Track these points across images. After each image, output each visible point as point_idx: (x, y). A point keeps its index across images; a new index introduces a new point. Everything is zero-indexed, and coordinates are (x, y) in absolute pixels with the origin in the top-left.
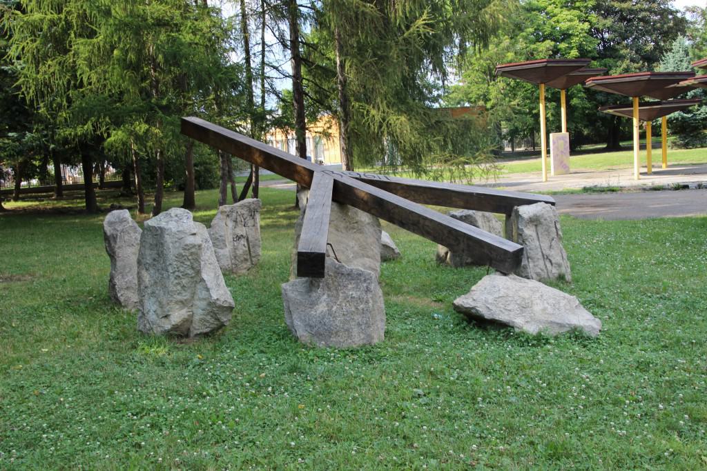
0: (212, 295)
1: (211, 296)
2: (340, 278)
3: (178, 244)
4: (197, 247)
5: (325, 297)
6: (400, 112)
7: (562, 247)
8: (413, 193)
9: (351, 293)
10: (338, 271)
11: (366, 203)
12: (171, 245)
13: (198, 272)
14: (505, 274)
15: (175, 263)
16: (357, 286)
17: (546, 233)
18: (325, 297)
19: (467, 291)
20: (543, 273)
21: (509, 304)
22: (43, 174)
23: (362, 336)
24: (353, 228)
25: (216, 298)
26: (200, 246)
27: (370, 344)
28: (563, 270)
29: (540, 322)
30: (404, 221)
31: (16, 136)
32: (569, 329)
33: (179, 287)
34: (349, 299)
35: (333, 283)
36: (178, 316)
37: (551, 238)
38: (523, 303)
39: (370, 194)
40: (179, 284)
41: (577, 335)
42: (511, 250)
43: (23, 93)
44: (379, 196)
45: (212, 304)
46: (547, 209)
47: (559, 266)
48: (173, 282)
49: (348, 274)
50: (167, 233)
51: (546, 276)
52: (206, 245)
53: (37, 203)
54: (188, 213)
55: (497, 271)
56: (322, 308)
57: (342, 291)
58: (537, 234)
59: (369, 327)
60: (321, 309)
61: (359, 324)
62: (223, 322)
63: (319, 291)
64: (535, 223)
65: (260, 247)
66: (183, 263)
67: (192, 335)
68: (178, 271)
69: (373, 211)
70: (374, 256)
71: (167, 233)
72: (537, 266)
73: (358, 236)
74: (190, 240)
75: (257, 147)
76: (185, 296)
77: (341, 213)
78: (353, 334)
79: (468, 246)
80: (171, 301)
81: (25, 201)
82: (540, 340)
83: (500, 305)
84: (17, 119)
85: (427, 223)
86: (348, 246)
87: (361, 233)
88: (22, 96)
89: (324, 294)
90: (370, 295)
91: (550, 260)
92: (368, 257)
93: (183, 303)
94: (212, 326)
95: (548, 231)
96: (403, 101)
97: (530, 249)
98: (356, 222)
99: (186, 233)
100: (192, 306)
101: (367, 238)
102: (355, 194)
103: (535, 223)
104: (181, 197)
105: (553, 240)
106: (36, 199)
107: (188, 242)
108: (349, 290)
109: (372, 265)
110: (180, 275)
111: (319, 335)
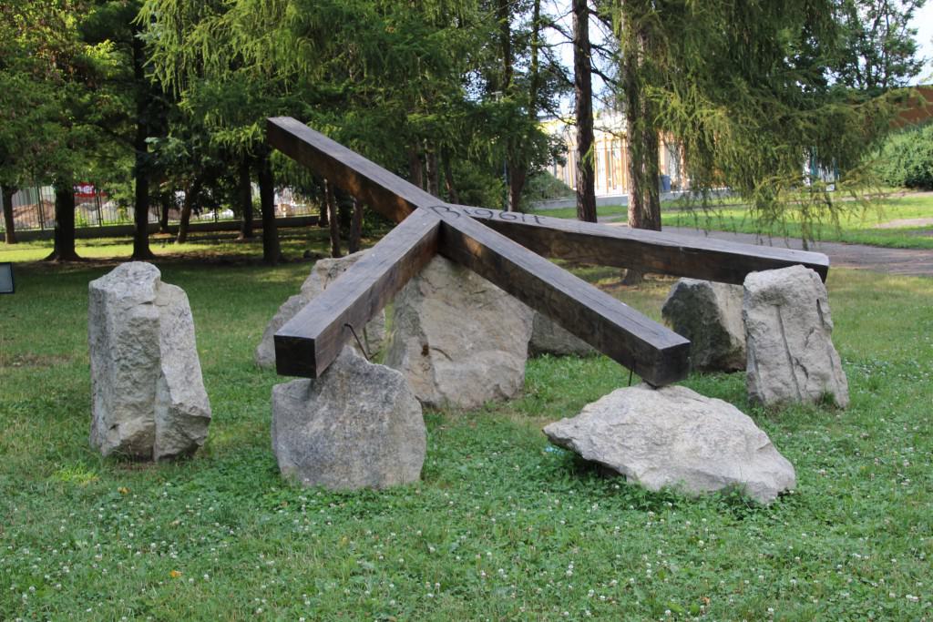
0: (173, 398)
1: (172, 400)
2: (354, 379)
3: (123, 317)
4: (151, 323)
5: (325, 408)
6: (718, 102)
7: (832, 345)
8: (576, 245)
9: (361, 404)
10: (354, 369)
11: (480, 260)
12: (114, 317)
13: (157, 362)
14: (655, 388)
15: (119, 346)
16: (374, 393)
17: (798, 319)
18: (325, 408)
19: (575, 409)
20: (785, 389)
21: (630, 438)
22: (242, 203)
23: (366, 473)
24: (477, 301)
25: (178, 402)
26: (155, 321)
27: (378, 486)
28: (831, 386)
29: (678, 470)
30: (526, 293)
31: (155, 142)
32: (723, 486)
33: (128, 384)
34: (356, 414)
35: (342, 387)
36: (130, 427)
37: (808, 328)
38: (657, 436)
39: (485, 247)
40: (127, 378)
41: (736, 501)
42: (660, 344)
43: (157, 77)
44: (496, 251)
45: (174, 411)
46: (801, 277)
47: (824, 378)
48: (118, 375)
49: (367, 375)
50: (109, 299)
51: (794, 394)
52: (180, 322)
53: (204, 247)
54: (153, 270)
55: (644, 381)
56: (317, 426)
57: (351, 401)
58: (781, 322)
59: (377, 459)
60: (315, 428)
61: (364, 455)
62: (194, 441)
63: (319, 398)
64: (775, 302)
65: (383, 326)
66: (131, 346)
67: (156, 457)
68: (125, 359)
69: (489, 274)
70: (515, 348)
71: (109, 299)
72: (775, 376)
73: (488, 314)
74: (142, 312)
75: (353, 167)
76: (140, 397)
77: (454, 276)
78: (353, 470)
79: (606, 338)
80: (119, 404)
81: (197, 243)
82: (657, 501)
83: (615, 437)
84: (160, 116)
85: (553, 296)
86: (464, 329)
87: (491, 309)
88: (156, 80)
89: (324, 404)
90: (388, 409)
91: (802, 366)
92: (503, 349)
93: (138, 408)
94: (180, 445)
95: (801, 316)
96: (722, 83)
97: (760, 347)
98: (483, 292)
99: (135, 301)
100: (153, 412)
101: (502, 318)
102: (465, 247)
103: (775, 302)
104: (50, 246)
105: (812, 332)
106: (215, 240)
107: (136, 315)
108: (361, 400)
109: (509, 363)
110: (128, 364)
111: (306, 468)
